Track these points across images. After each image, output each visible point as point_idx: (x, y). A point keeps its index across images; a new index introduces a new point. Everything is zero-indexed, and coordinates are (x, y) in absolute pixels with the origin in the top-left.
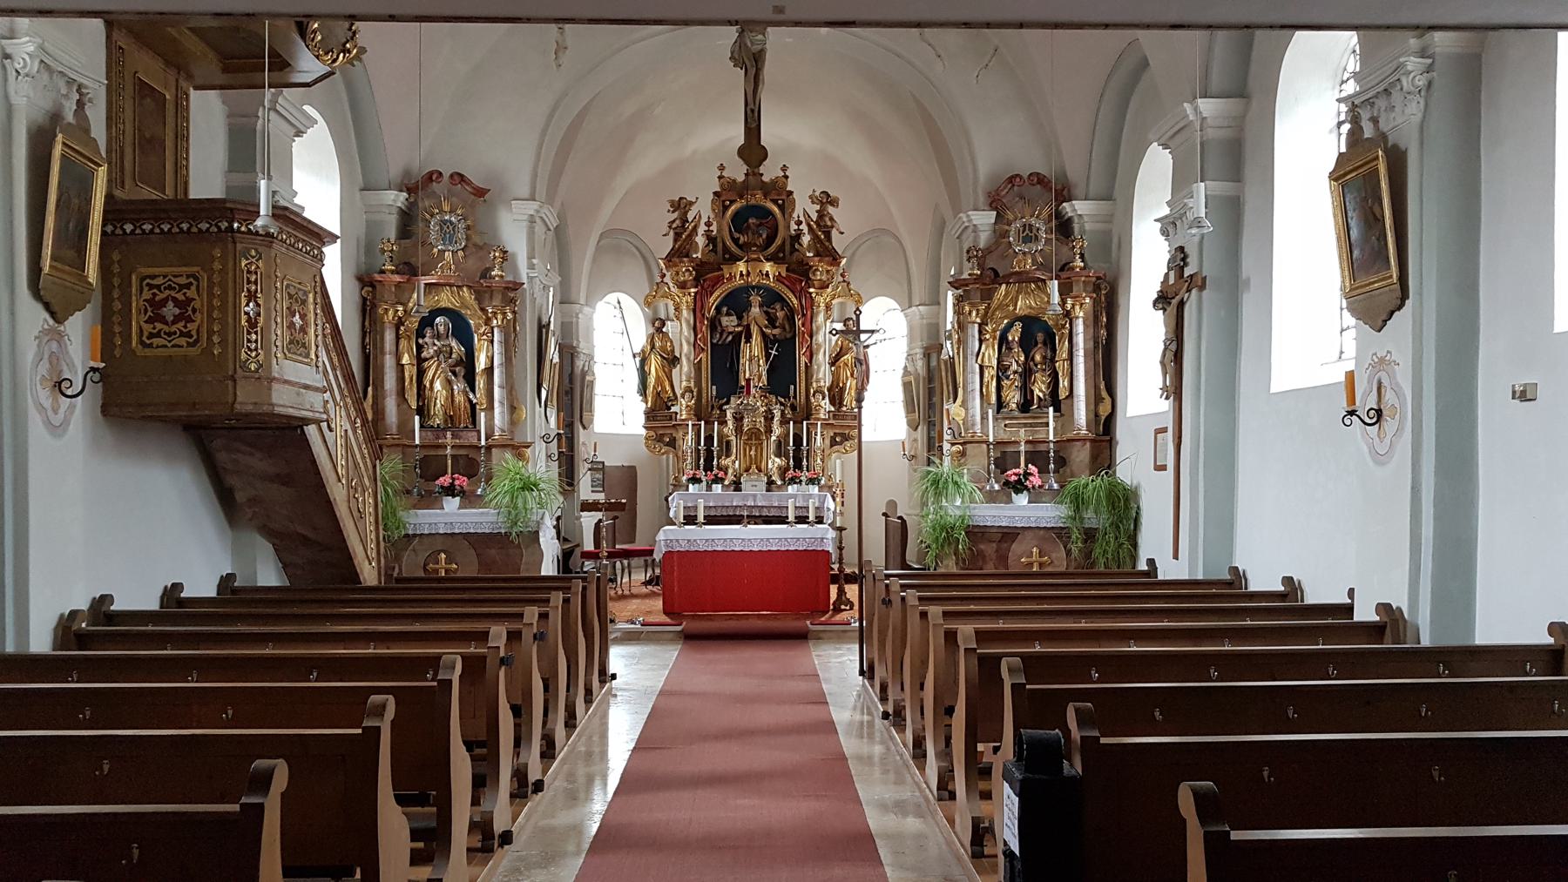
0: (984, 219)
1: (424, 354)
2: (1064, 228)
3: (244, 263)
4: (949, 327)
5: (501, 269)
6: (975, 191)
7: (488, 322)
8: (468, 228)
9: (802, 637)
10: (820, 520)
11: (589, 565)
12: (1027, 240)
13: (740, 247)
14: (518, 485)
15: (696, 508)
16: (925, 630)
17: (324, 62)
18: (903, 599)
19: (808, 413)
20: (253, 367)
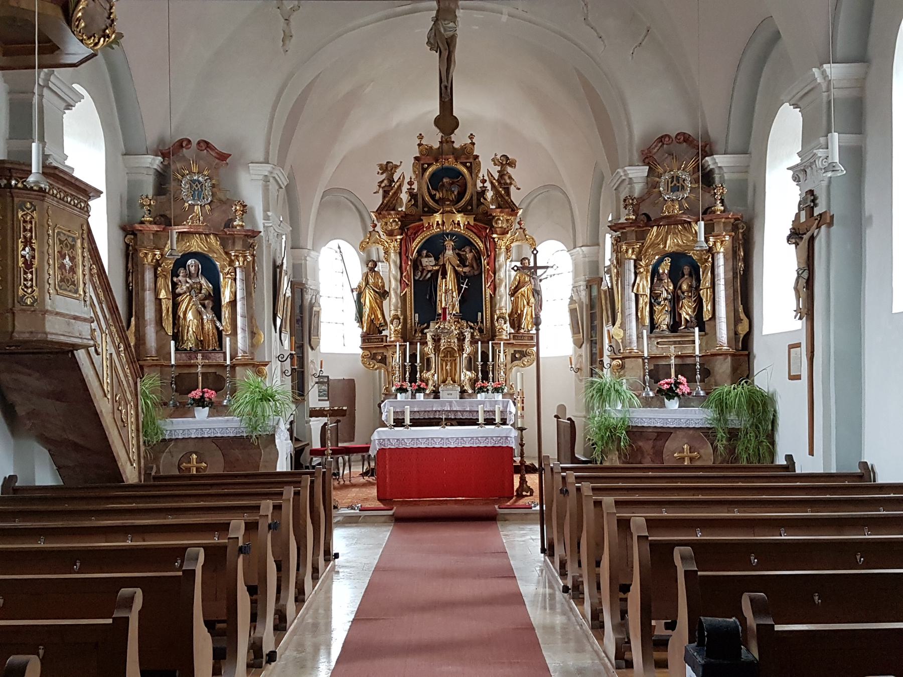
0: (639, 173)
1: (178, 290)
2: (707, 178)
3: (20, 214)
4: (607, 263)
5: (242, 220)
6: (630, 151)
7: (231, 263)
8: (213, 186)
9: (491, 519)
10: (504, 422)
11: (316, 460)
12: (675, 189)
13: (436, 201)
14: (257, 396)
15: (403, 413)
16: (599, 516)
17: (87, 45)
18: (578, 489)
19: (492, 334)
20: (29, 301)
